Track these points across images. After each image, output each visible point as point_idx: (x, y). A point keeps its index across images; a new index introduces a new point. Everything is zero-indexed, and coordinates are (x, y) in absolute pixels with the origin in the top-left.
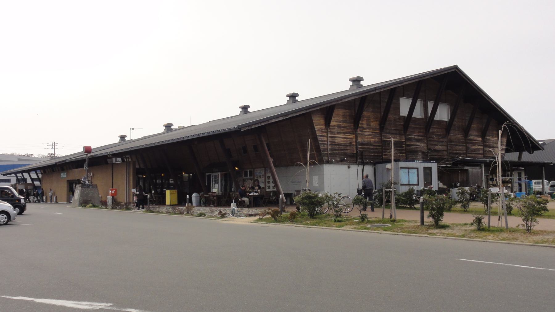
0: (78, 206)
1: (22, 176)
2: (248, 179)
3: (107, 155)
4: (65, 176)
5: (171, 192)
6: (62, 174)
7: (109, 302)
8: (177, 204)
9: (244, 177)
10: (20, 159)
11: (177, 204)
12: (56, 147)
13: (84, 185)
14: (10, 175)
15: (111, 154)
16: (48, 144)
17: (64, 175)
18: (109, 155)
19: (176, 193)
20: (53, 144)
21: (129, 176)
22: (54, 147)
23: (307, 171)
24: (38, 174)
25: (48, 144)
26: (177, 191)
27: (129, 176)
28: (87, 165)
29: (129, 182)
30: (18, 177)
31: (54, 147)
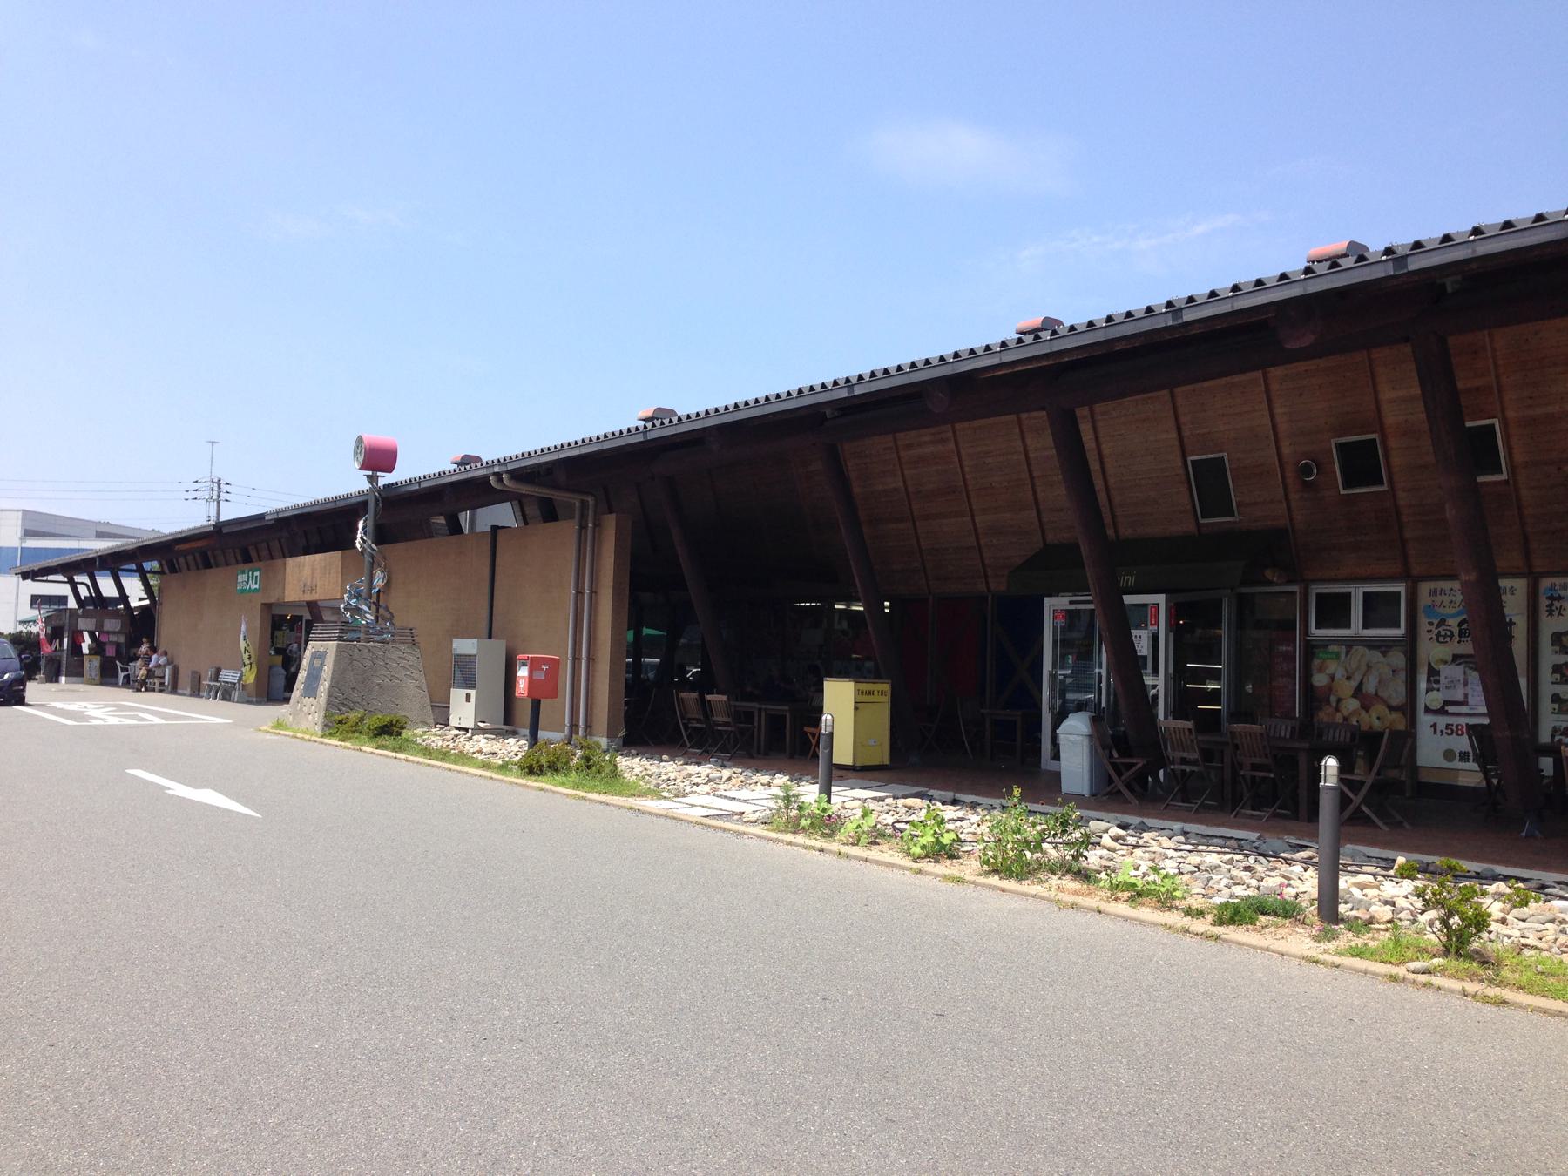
0: (318, 729)
1: (88, 582)
2: (1350, 644)
3: (485, 479)
4: (257, 586)
5: (858, 692)
6: (242, 578)
7: (229, 719)
8: (887, 762)
9: (1313, 630)
10: (102, 532)
11: (887, 762)
12: (224, 496)
13: (347, 631)
14: (45, 578)
15: (508, 472)
16: (196, 486)
17: (248, 580)
18: (498, 475)
19: (886, 699)
20: (216, 488)
21: (593, 592)
22: (219, 496)
23: (1151, 618)
24: (148, 575)
25: (196, 486)
26: (885, 687)
27: (593, 592)
28: (370, 528)
29: (590, 616)
30: (66, 580)
31: (219, 496)
